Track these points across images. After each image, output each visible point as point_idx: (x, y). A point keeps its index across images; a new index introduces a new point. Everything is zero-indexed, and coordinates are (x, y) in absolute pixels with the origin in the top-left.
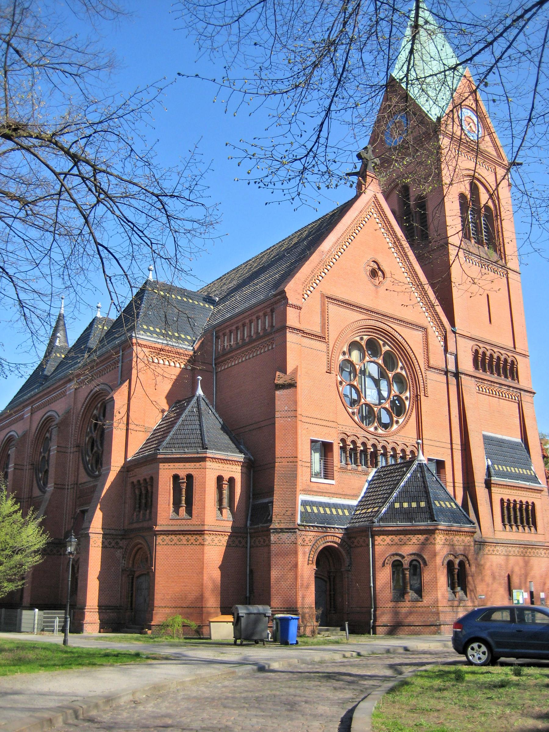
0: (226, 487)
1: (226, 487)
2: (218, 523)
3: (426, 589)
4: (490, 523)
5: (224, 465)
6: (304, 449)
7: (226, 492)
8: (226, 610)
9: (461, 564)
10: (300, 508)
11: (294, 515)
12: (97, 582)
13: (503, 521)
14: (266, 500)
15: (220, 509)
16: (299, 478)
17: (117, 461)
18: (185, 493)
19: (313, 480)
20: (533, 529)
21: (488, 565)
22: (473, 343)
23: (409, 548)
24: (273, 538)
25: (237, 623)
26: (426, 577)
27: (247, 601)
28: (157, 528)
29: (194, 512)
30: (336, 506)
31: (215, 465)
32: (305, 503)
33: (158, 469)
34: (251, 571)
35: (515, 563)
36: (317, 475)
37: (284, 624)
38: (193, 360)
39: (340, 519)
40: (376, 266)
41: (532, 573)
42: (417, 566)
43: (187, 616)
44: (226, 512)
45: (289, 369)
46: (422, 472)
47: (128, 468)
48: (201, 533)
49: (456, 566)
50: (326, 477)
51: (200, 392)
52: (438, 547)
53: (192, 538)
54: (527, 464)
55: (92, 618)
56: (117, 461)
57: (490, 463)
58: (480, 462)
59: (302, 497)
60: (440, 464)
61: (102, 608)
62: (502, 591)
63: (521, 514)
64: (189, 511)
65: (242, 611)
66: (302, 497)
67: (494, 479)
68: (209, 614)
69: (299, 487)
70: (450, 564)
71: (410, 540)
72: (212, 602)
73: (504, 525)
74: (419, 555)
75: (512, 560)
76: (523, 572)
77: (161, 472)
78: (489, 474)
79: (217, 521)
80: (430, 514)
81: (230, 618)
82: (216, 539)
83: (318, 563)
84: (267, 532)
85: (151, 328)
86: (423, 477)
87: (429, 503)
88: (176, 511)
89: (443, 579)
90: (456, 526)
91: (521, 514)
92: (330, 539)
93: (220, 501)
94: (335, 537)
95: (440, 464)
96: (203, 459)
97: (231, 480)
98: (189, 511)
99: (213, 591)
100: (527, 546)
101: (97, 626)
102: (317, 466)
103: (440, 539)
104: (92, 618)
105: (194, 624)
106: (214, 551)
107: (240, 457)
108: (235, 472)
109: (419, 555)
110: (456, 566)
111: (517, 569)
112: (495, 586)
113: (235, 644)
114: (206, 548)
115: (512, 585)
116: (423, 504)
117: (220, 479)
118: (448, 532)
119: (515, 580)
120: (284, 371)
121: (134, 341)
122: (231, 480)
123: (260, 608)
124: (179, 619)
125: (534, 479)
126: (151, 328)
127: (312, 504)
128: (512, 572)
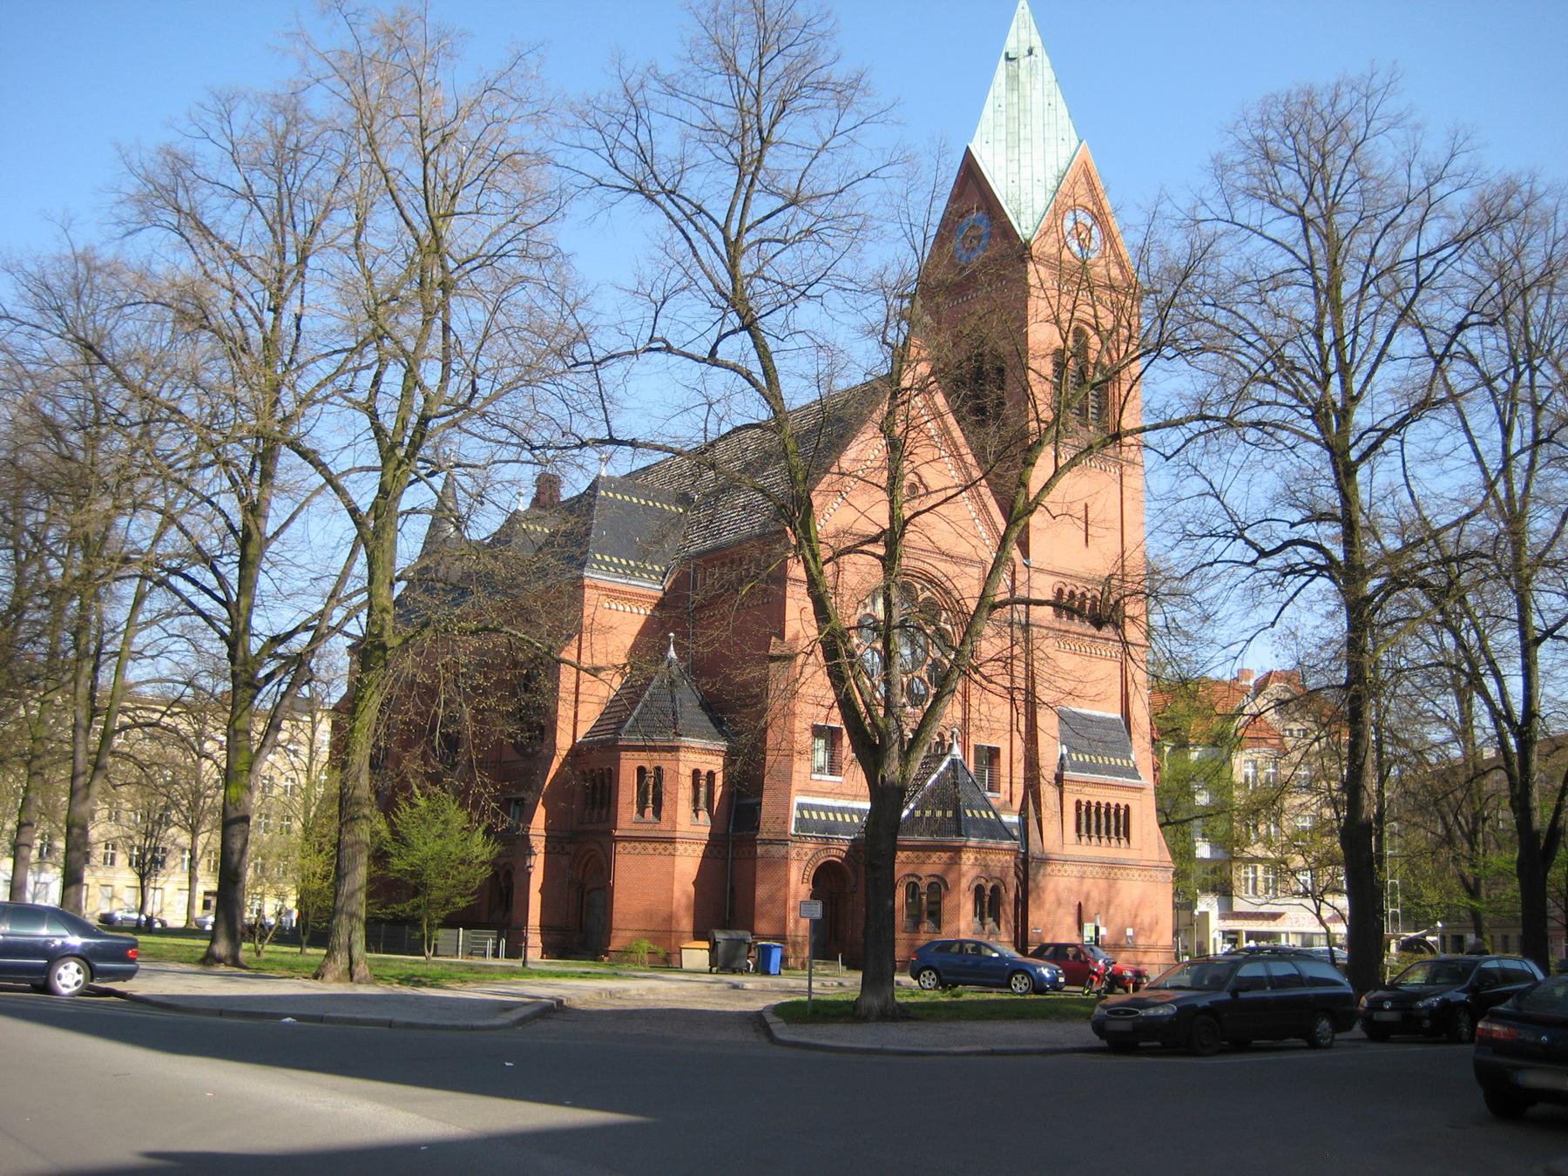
0: (703, 782)
1: (703, 782)
2: (693, 829)
3: (945, 917)
4: (1057, 833)
5: (701, 754)
6: (804, 738)
7: (703, 790)
8: (699, 935)
9: (995, 889)
10: (795, 813)
11: (786, 822)
12: (539, 896)
13: (1078, 829)
14: (751, 801)
15: (696, 811)
16: (795, 776)
17: (564, 742)
18: (653, 793)
19: (816, 777)
20: (1123, 842)
21: (1050, 886)
22: (1053, 580)
23: (934, 864)
24: (759, 850)
25: (713, 950)
26: (947, 903)
27: (725, 926)
28: (617, 833)
29: (663, 814)
30: (842, 810)
31: (691, 756)
32: (801, 807)
33: (619, 759)
34: (732, 889)
35: (1094, 887)
36: (820, 770)
37: (766, 952)
38: (661, 605)
39: (847, 828)
40: (916, 479)
41: (1117, 901)
42: (939, 887)
43: (655, 940)
44: (704, 816)
45: (789, 634)
46: (955, 771)
47: (576, 751)
48: (672, 841)
49: (988, 892)
50: (832, 773)
51: (672, 653)
52: (964, 868)
53: (660, 847)
54: (1125, 752)
55: (534, 939)
56: (564, 742)
57: (1065, 751)
58: (1051, 752)
59: (798, 799)
60: (994, 753)
61: (544, 928)
62: (1070, 920)
63: (1108, 821)
64: (657, 812)
65: (720, 936)
66: (798, 799)
67: (1068, 774)
68: (680, 939)
69: (795, 785)
70: (979, 890)
71: (929, 857)
72: (686, 923)
73: (1080, 836)
74: (941, 879)
75: (1088, 883)
76: (1104, 899)
77: (623, 762)
78: (1062, 766)
79: (691, 826)
80: (958, 826)
81: (706, 945)
82: (690, 849)
83: (815, 882)
84: (753, 842)
85: (607, 558)
86: (955, 777)
87: (957, 812)
88: (641, 812)
89: (968, 906)
90: (991, 843)
91: (1108, 821)
92: (834, 852)
93: (696, 800)
94: (839, 848)
95: (994, 753)
96: (676, 749)
97: (711, 774)
98: (657, 812)
99: (687, 909)
100: (1112, 867)
101: (539, 951)
102: (821, 757)
103: (968, 858)
104: (534, 939)
105: (662, 952)
106: (687, 863)
107: (722, 745)
108: (716, 764)
109: (941, 879)
110: (988, 892)
111: (1095, 894)
112: (1061, 911)
113: (710, 972)
114: (678, 859)
115: (1084, 916)
116: (950, 814)
117: (696, 773)
118: (979, 849)
119: (1091, 909)
120: (781, 635)
121: (587, 582)
122: (711, 774)
123: (741, 934)
124: (645, 944)
125: (1133, 773)
126: (607, 558)
127: (811, 807)
128: (1087, 898)
